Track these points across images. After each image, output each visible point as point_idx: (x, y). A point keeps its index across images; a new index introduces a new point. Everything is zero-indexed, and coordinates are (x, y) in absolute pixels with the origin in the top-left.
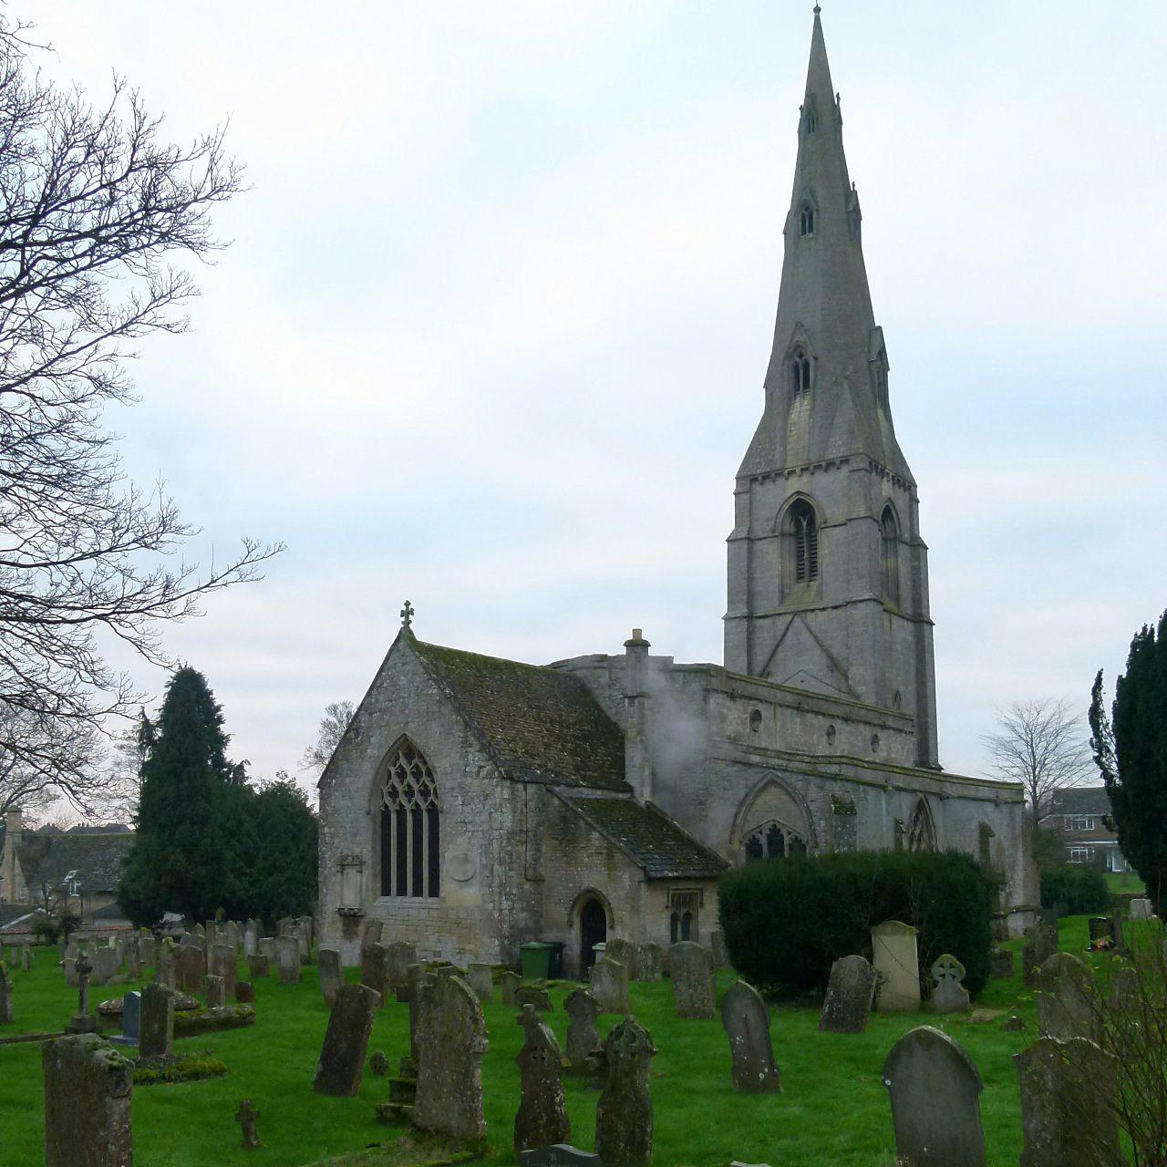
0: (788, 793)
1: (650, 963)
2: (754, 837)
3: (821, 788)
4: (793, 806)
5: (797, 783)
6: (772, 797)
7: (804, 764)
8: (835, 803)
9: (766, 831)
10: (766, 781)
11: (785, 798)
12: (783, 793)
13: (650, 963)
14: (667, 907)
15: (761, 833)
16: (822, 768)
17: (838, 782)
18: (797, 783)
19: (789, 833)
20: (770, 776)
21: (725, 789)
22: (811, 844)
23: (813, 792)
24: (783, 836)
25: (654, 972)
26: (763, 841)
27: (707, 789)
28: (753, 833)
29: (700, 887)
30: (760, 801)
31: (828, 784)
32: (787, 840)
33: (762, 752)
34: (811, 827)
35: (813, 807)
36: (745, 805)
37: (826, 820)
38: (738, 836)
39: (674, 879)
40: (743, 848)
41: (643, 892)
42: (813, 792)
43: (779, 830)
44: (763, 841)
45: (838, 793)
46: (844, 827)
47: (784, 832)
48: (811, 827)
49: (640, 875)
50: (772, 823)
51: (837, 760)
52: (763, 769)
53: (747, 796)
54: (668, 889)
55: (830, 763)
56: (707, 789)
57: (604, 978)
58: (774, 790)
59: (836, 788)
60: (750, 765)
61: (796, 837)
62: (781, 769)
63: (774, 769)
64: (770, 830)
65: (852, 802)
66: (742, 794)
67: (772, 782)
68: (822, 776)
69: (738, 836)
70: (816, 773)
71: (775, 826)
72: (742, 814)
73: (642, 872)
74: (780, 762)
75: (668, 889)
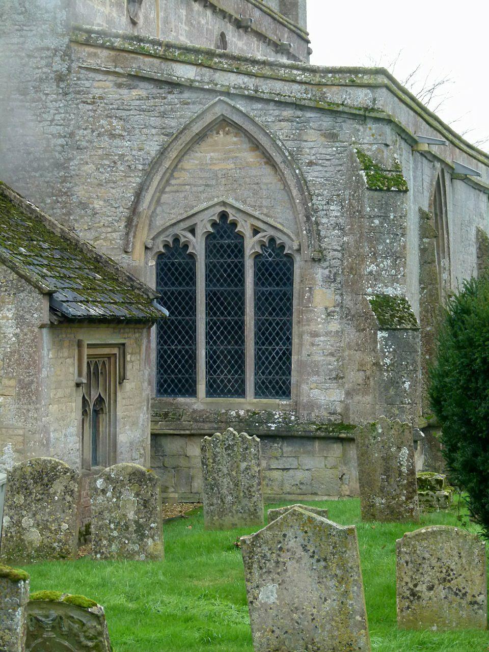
0: (256, 146)
1: (131, 515)
2: (176, 240)
3: (332, 137)
4: (266, 175)
5: (279, 126)
6: (221, 156)
7: (296, 87)
8: (367, 168)
9: (204, 227)
10: (209, 118)
11: (251, 157)
12: (246, 145)
13: (131, 515)
14: (78, 385)
15: (192, 231)
16: (334, 96)
17: (370, 124)
18: (279, 126)
19: (256, 231)
20: (219, 110)
21: (113, 136)
22: (308, 253)
23: (314, 144)
24: (240, 236)
25: (143, 536)
26: (198, 246)
27: (72, 135)
28: (177, 230)
29: (122, 341)
30: (190, 163)
31: (347, 128)
32: (251, 246)
33: (201, 58)
34: (308, 218)
35: (312, 175)
36: (161, 167)
37: (341, 203)
38: (143, 236)
39: (90, 321)
40: (152, 263)
41: (45, 352)
42: (314, 144)
43: (234, 224)
44: (198, 246)
45: (370, 150)
46: (385, 217)
47: (244, 227)
48: (308, 218)
49: (41, 312)
50: (220, 209)
51: (366, 79)
52: (201, 95)
53: (163, 152)
54: (80, 344)
55: (353, 84)
56: (72, 135)
57: (291, 565)
58: (224, 140)
59: (367, 138)
60: (174, 85)
61: (272, 240)
62: (244, 96)
63: (228, 94)
64: (214, 224)
65: (397, 168)
66: (153, 148)
67: (224, 123)
68: (333, 112)
69: (143, 236)
70: (322, 104)
71: (224, 216)
72: (151, 190)
73: (46, 305)
74: (241, 80)
75: (80, 344)
